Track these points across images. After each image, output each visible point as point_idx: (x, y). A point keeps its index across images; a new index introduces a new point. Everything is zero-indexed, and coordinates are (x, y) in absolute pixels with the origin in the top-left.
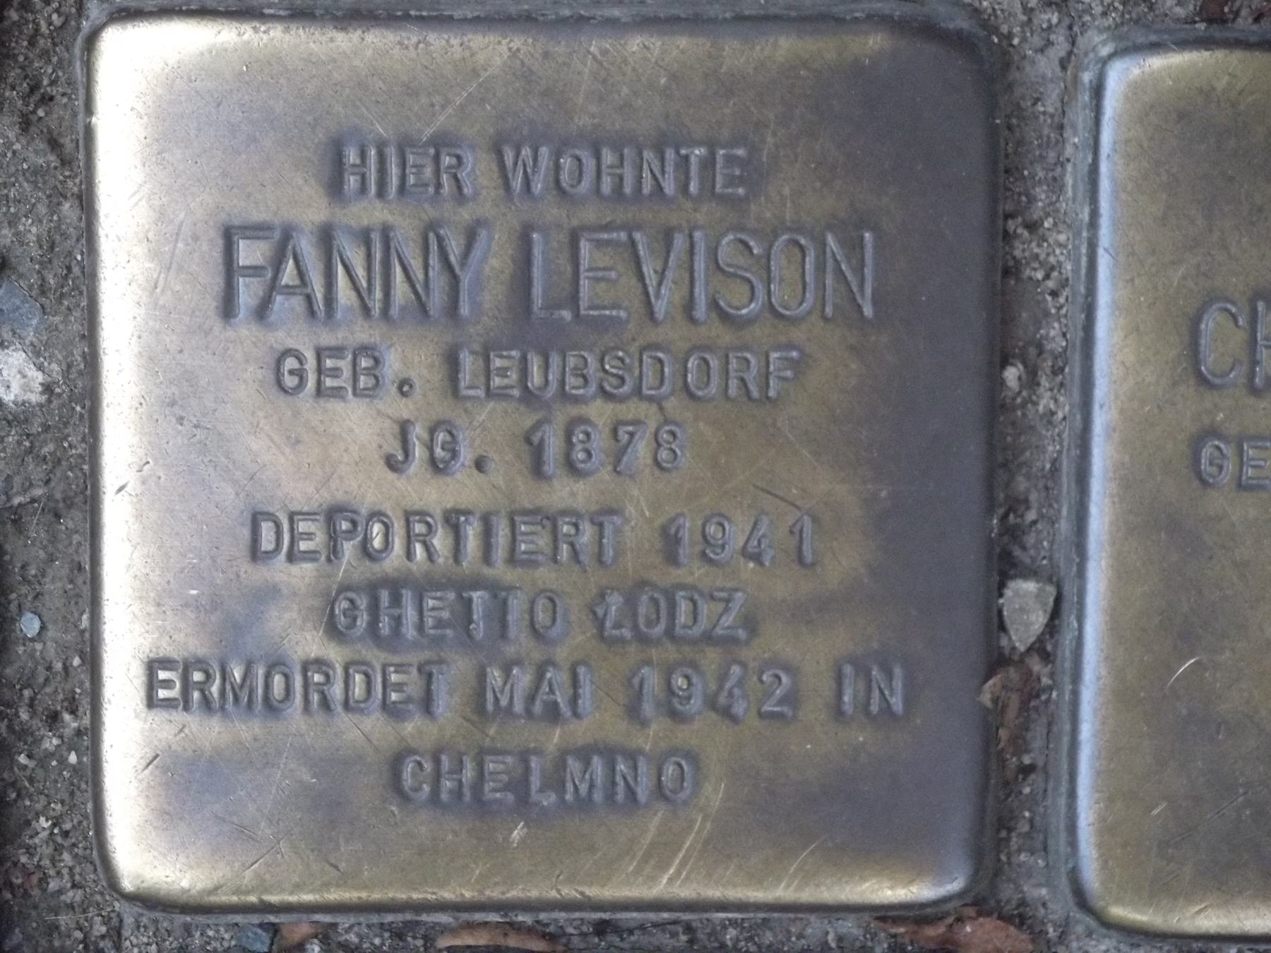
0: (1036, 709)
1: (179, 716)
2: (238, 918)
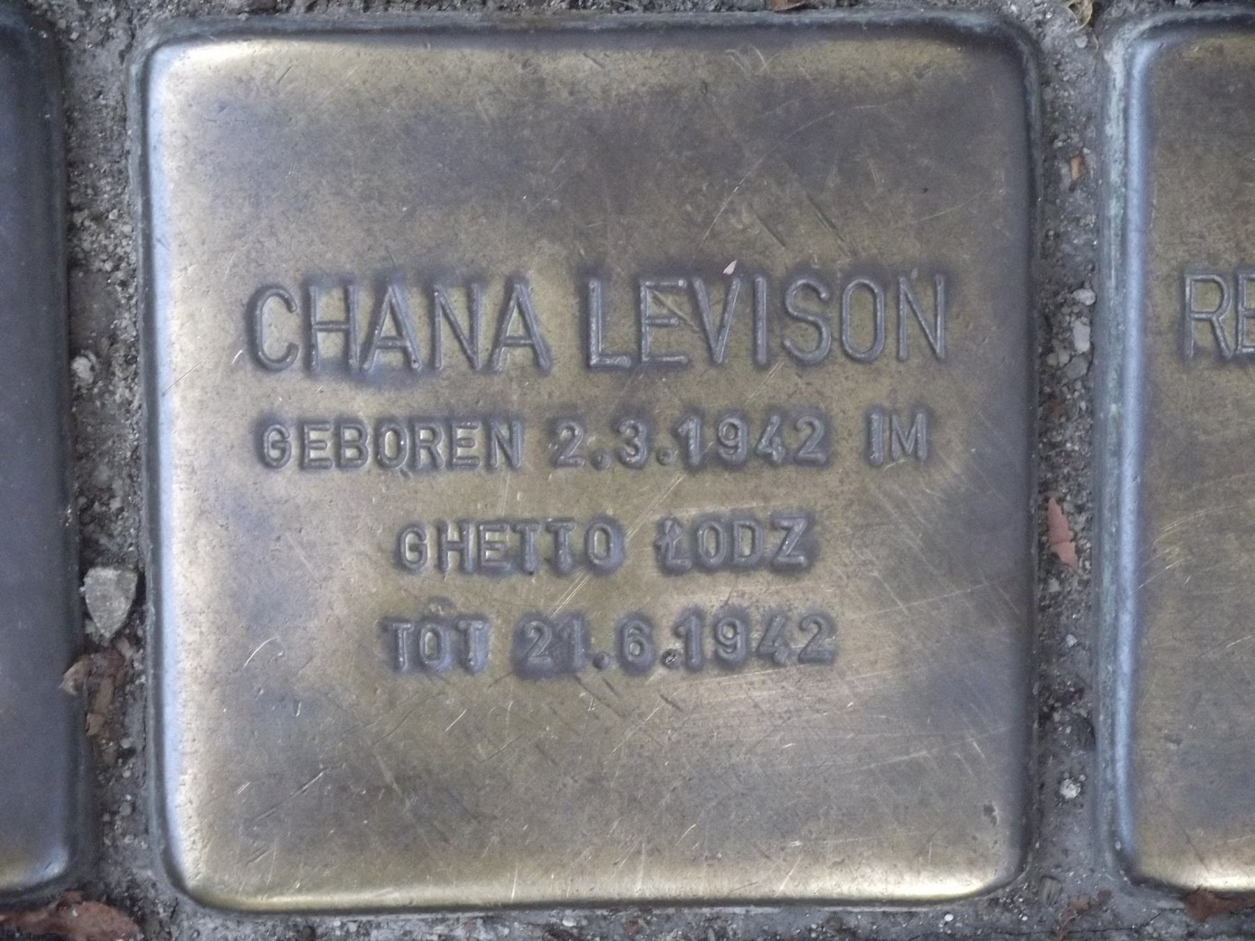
0: (132, 693)
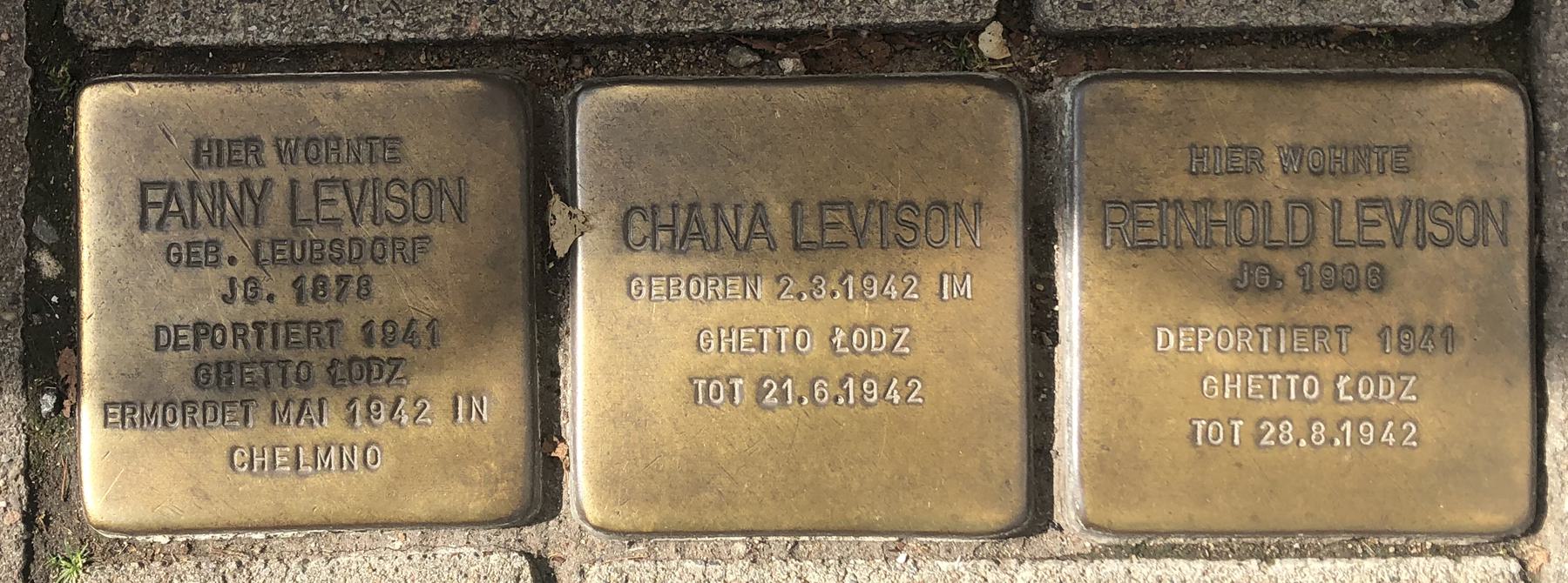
1: (119, 431)
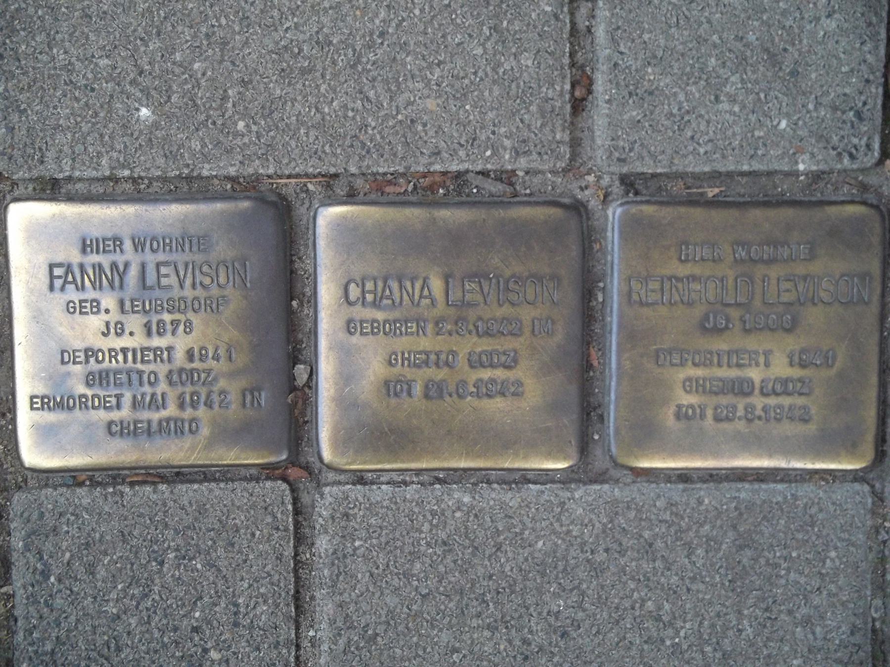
1: (40, 412)
2: (62, 474)
